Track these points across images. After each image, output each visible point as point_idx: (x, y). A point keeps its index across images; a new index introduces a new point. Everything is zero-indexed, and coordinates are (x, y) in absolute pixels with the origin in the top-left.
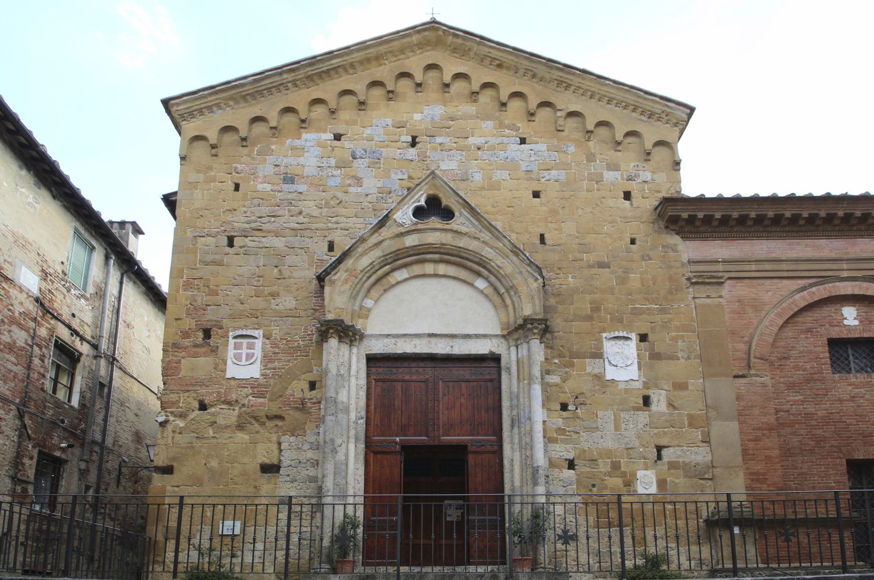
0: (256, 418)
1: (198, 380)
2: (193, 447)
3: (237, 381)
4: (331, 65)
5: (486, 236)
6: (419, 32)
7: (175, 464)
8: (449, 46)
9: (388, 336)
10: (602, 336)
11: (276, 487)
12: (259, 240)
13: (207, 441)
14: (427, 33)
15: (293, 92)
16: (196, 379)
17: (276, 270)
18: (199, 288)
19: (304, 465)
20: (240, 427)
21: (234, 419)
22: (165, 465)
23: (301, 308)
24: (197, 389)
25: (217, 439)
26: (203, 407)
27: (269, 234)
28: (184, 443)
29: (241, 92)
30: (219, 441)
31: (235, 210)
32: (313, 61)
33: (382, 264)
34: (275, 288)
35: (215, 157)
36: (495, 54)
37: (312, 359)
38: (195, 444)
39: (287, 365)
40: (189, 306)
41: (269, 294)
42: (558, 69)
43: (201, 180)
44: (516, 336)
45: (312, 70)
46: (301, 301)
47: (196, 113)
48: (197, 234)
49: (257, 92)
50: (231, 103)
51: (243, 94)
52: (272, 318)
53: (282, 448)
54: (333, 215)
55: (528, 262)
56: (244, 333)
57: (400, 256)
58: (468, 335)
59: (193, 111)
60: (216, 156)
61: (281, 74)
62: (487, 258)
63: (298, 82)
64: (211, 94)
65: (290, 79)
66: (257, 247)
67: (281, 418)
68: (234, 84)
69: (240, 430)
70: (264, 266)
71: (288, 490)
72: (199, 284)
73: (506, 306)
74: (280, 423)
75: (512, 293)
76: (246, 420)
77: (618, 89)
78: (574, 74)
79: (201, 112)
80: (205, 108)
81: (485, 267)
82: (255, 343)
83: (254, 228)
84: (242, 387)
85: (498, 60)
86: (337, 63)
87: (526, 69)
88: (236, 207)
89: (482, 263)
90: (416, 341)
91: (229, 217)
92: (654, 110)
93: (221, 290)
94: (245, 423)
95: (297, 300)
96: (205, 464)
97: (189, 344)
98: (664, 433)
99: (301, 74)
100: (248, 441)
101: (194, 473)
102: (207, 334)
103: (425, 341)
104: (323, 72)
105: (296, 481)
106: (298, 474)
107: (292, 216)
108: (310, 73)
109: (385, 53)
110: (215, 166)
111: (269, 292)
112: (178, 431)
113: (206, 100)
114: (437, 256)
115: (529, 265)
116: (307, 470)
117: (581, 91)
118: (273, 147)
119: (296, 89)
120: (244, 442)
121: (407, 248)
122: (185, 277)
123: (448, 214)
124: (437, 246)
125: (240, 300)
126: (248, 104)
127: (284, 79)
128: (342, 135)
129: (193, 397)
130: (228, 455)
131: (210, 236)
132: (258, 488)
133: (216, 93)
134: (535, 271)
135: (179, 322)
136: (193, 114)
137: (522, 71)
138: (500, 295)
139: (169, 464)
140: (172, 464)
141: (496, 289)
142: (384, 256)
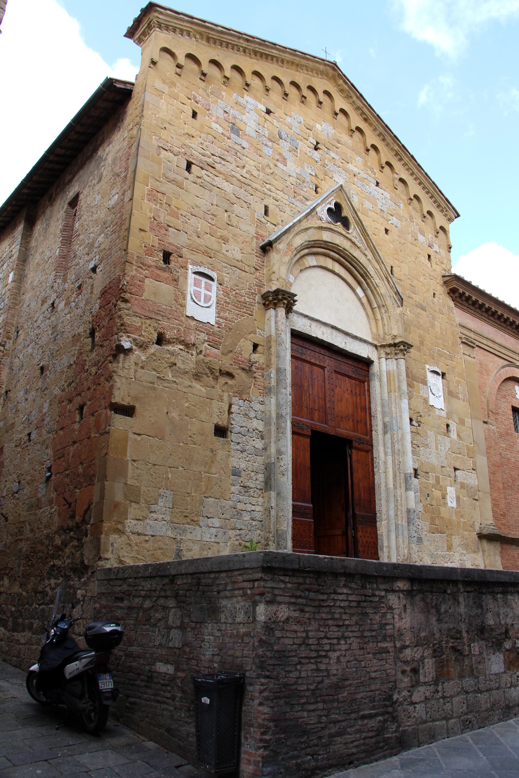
0: (211, 370)
1: (160, 309)
2: (155, 389)
3: (195, 323)
4: (272, 52)
5: (370, 256)
6: (325, 65)
7: (137, 406)
8: (339, 85)
9: (306, 316)
10: (425, 366)
11: (229, 455)
12: (213, 177)
13: (168, 385)
14: (328, 68)
15: (240, 54)
16: (158, 307)
17: (226, 215)
18: (161, 204)
19: (251, 435)
20: (197, 376)
21: (192, 365)
22: (126, 404)
23: (246, 263)
24: (158, 318)
25: (177, 384)
26: (160, 340)
27: (220, 175)
28: (147, 381)
29: (209, 33)
30: (179, 387)
31: (193, 137)
32: (263, 43)
33: (307, 246)
34: (225, 233)
35: (177, 76)
36: (365, 110)
37: (255, 320)
38: (156, 386)
39: (237, 319)
40: (152, 219)
41: (221, 236)
42: (398, 145)
43: (166, 92)
44: (388, 350)
45: (259, 49)
46: (246, 255)
47: (171, 28)
48: (161, 145)
49: (220, 40)
50: (198, 37)
51: (210, 36)
52: (223, 264)
53: (233, 410)
54: (267, 182)
55: (395, 290)
56: (206, 272)
57: (316, 245)
58: (356, 336)
59: (170, 26)
60: (180, 76)
61: (240, 38)
62: (370, 274)
63: (247, 50)
64: (188, 22)
65: (244, 46)
66: (211, 184)
67: (230, 375)
68: (207, 24)
69: (196, 379)
70: (217, 206)
71: (239, 460)
72: (162, 199)
73: (376, 320)
74: (230, 382)
75: (383, 311)
76: (204, 370)
77: (426, 179)
78: (406, 154)
79: (174, 30)
80: (179, 28)
81: (365, 280)
82: (211, 285)
83: (209, 163)
84: (199, 331)
85: (367, 116)
86: (275, 53)
87: (381, 133)
88: (194, 135)
89: (365, 275)
90: (324, 329)
91: (187, 142)
92: (441, 204)
93: (181, 215)
94: (202, 374)
95: (243, 253)
96: (167, 413)
97: (152, 264)
98: (458, 458)
99: (251, 46)
100: (205, 395)
101: (156, 422)
102: (167, 257)
103: (329, 330)
104: (265, 54)
105: (245, 451)
106: (247, 443)
107: (238, 167)
108: (257, 49)
109: (303, 65)
110: (178, 84)
111: (221, 234)
112: (140, 365)
113: (182, 23)
114: (337, 256)
115: (395, 294)
116: (254, 440)
117: (407, 167)
118: (224, 93)
119: (243, 53)
120: (202, 395)
121: (323, 241)
122: (150, 187)
123: (346, 223)
124: (341, 249)
125: (197, 232)
126: (209, 44)
127: (240, 43)
128: (272, 112)
129: (154, 327)
130: (187, 407)
131: (172, 152)
132: (215, 453)
133: (192, 23)
134: (399, 300)
135: (142, 233)
136: (168, 28)
137: (378, 132)
138: (372, 309)
139: (131, 404)
140: (135, 404)
141: (369, 300)
142: (309, 241)
